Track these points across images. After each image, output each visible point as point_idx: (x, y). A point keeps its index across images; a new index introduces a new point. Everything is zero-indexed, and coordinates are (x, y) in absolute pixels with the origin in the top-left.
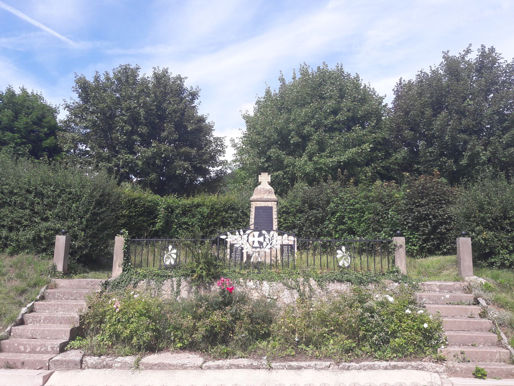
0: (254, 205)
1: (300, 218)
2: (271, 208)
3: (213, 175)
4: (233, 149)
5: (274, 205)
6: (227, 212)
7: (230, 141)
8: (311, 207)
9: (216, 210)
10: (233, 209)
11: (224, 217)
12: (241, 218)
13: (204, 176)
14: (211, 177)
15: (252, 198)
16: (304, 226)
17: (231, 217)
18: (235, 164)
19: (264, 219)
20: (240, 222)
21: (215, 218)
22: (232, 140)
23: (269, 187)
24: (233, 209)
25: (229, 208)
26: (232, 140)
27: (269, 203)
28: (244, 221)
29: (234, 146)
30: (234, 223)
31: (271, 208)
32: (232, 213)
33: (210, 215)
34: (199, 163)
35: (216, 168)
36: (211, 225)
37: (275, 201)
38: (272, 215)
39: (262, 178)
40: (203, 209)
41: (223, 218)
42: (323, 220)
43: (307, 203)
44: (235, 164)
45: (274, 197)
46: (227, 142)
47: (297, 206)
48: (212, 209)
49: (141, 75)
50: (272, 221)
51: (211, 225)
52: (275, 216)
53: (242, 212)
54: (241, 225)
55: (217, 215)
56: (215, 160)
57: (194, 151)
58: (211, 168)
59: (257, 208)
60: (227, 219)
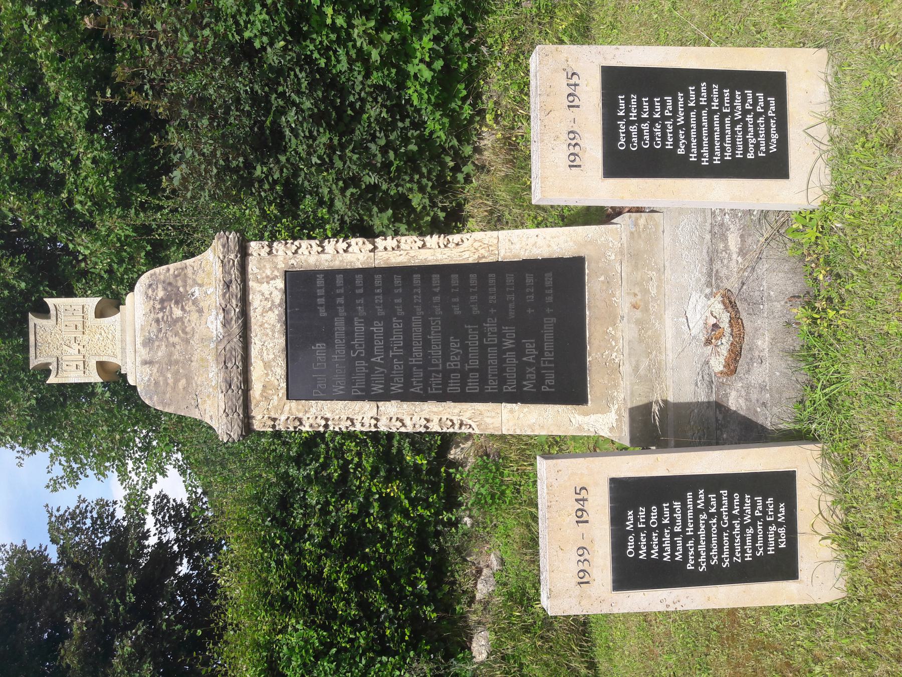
0: (276, 408)
1: (321, 203)
2: (298, 283)
3: (171, 534)
4: (83, 481)
5: (273, 263)
6: (300, 534)
7: (55, 490)
8: (269, 142)
9: (292, 586)
10: (284, 504)
11: (325, 544)
12: (325, 466)
13: (173, 561)
14: (177, 540)
15: (224, 428)
16: (354, 181)
17: (324, 512)
18: (133, 475)
19: (378, 328)
20: (344, 468)
21: (332, 590)
22: (55, 485)
23: (136, 303)
24: (284, 504)
25: (281, 523)
26: (55, 485)
27: (255, 300)
28: (340, 451)
29: (73, 477)
30: (347, 495)
31: (298, 283)
32: (306, 506)
33: (319, 614)
34: (122, 597)
35: (150, 522)
36: (363, 605)
37: (244, 253)
38: (349, 274)
39: (71, 354)
40: (291, 649)
41: (329, 547)
42: (329, 83)
43: (249, 166)
44: (133, 475)
45: (209, 265)
46: (66, 500)
47: (264, 215)
48: (287, 606)
49: (429, 236)
50: (389, 272)
51: (363, 605)
52: (356, 254)
53: (299, 461)
54: (359, 465)
55: (316, 579)
56: (127, 529)
57: (77, 624)
58: (152, 541)
59: (298, 386)
60: (335, 527)
